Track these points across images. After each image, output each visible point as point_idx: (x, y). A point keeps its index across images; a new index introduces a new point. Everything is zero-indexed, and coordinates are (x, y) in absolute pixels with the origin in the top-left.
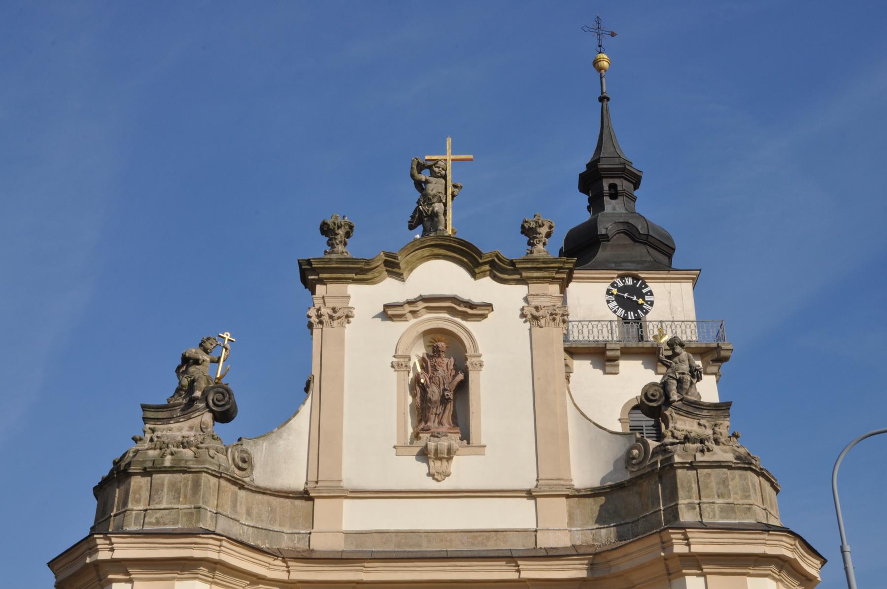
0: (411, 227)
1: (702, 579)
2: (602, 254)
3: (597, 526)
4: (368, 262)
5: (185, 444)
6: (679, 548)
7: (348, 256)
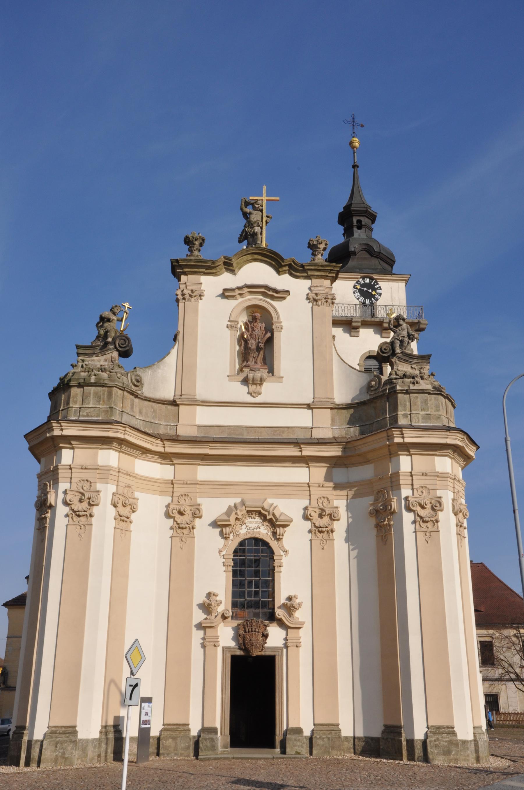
0: (240, 241)
1: (410, 457)
2: (352, 263)
3: (348, 426)
4: (214, 262)
5: (103, 370)
6: (398, 440)
7: (201, 258)
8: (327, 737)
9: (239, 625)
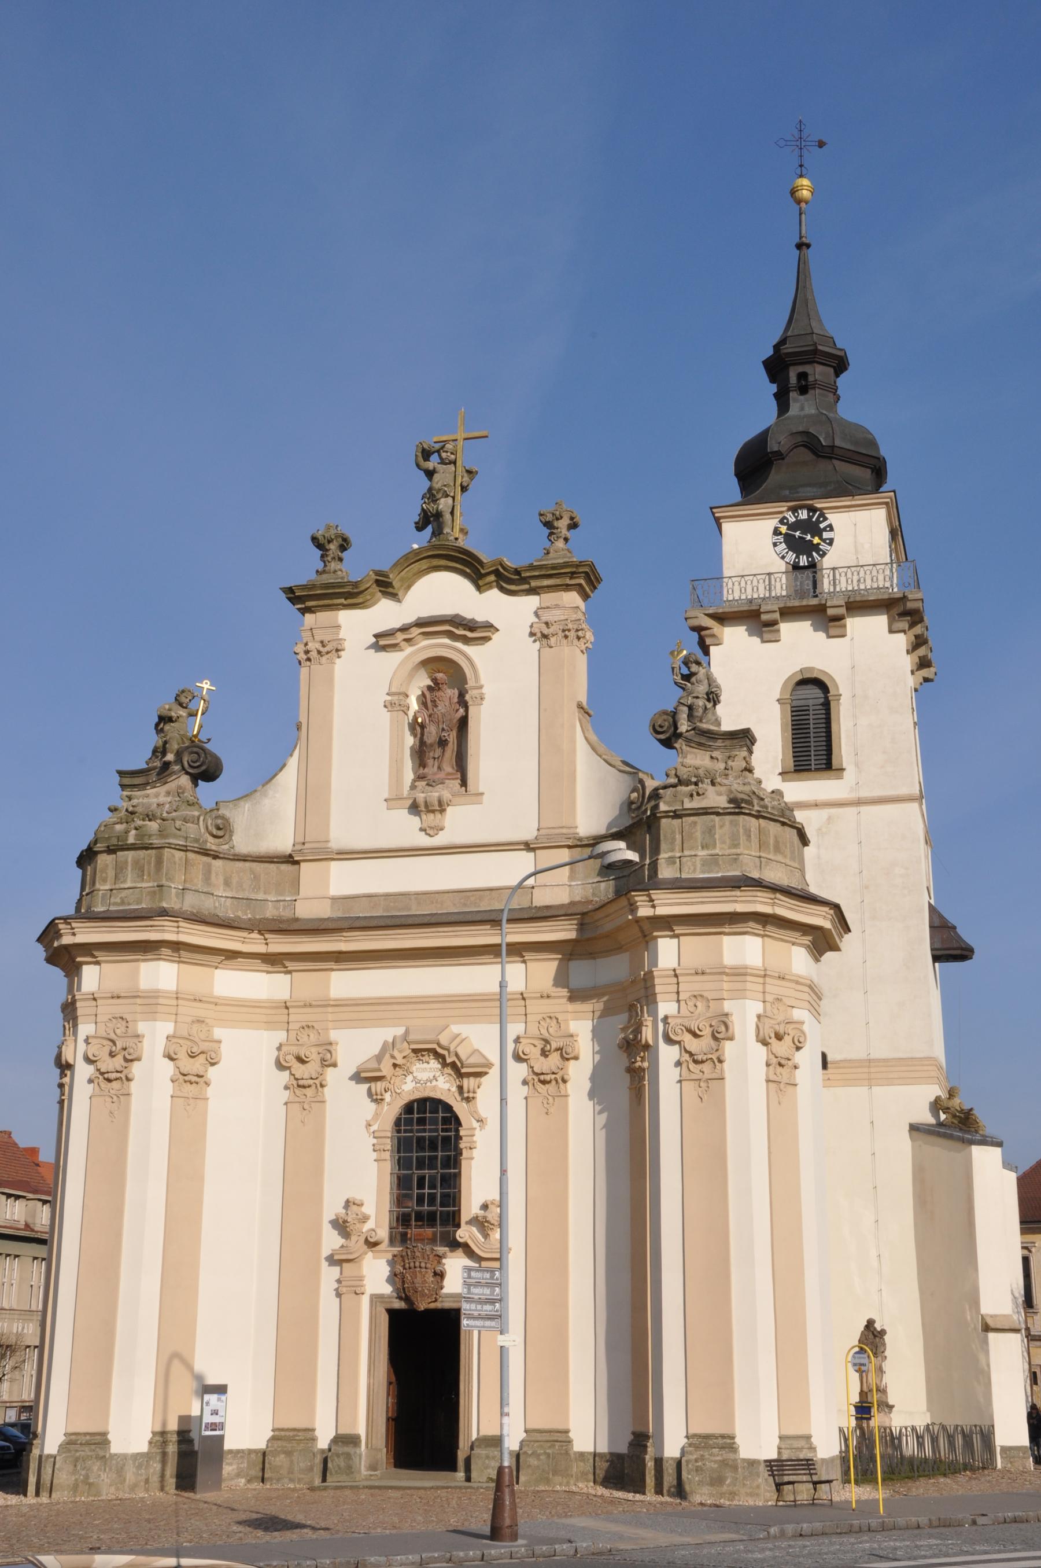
2: (775, 477)
3: (599, 879)
4: (356, 584)
6: (644, 911)
8: (545, 1453)
9: (394, 1256)
